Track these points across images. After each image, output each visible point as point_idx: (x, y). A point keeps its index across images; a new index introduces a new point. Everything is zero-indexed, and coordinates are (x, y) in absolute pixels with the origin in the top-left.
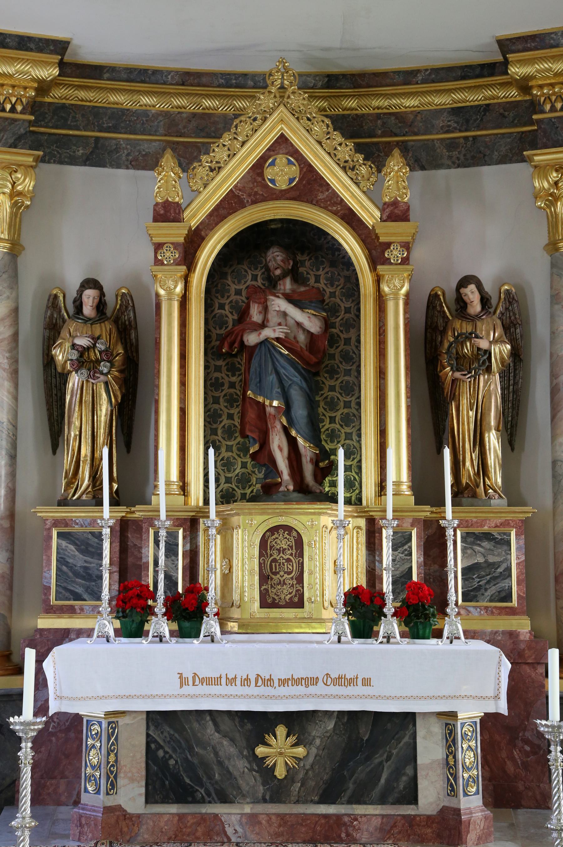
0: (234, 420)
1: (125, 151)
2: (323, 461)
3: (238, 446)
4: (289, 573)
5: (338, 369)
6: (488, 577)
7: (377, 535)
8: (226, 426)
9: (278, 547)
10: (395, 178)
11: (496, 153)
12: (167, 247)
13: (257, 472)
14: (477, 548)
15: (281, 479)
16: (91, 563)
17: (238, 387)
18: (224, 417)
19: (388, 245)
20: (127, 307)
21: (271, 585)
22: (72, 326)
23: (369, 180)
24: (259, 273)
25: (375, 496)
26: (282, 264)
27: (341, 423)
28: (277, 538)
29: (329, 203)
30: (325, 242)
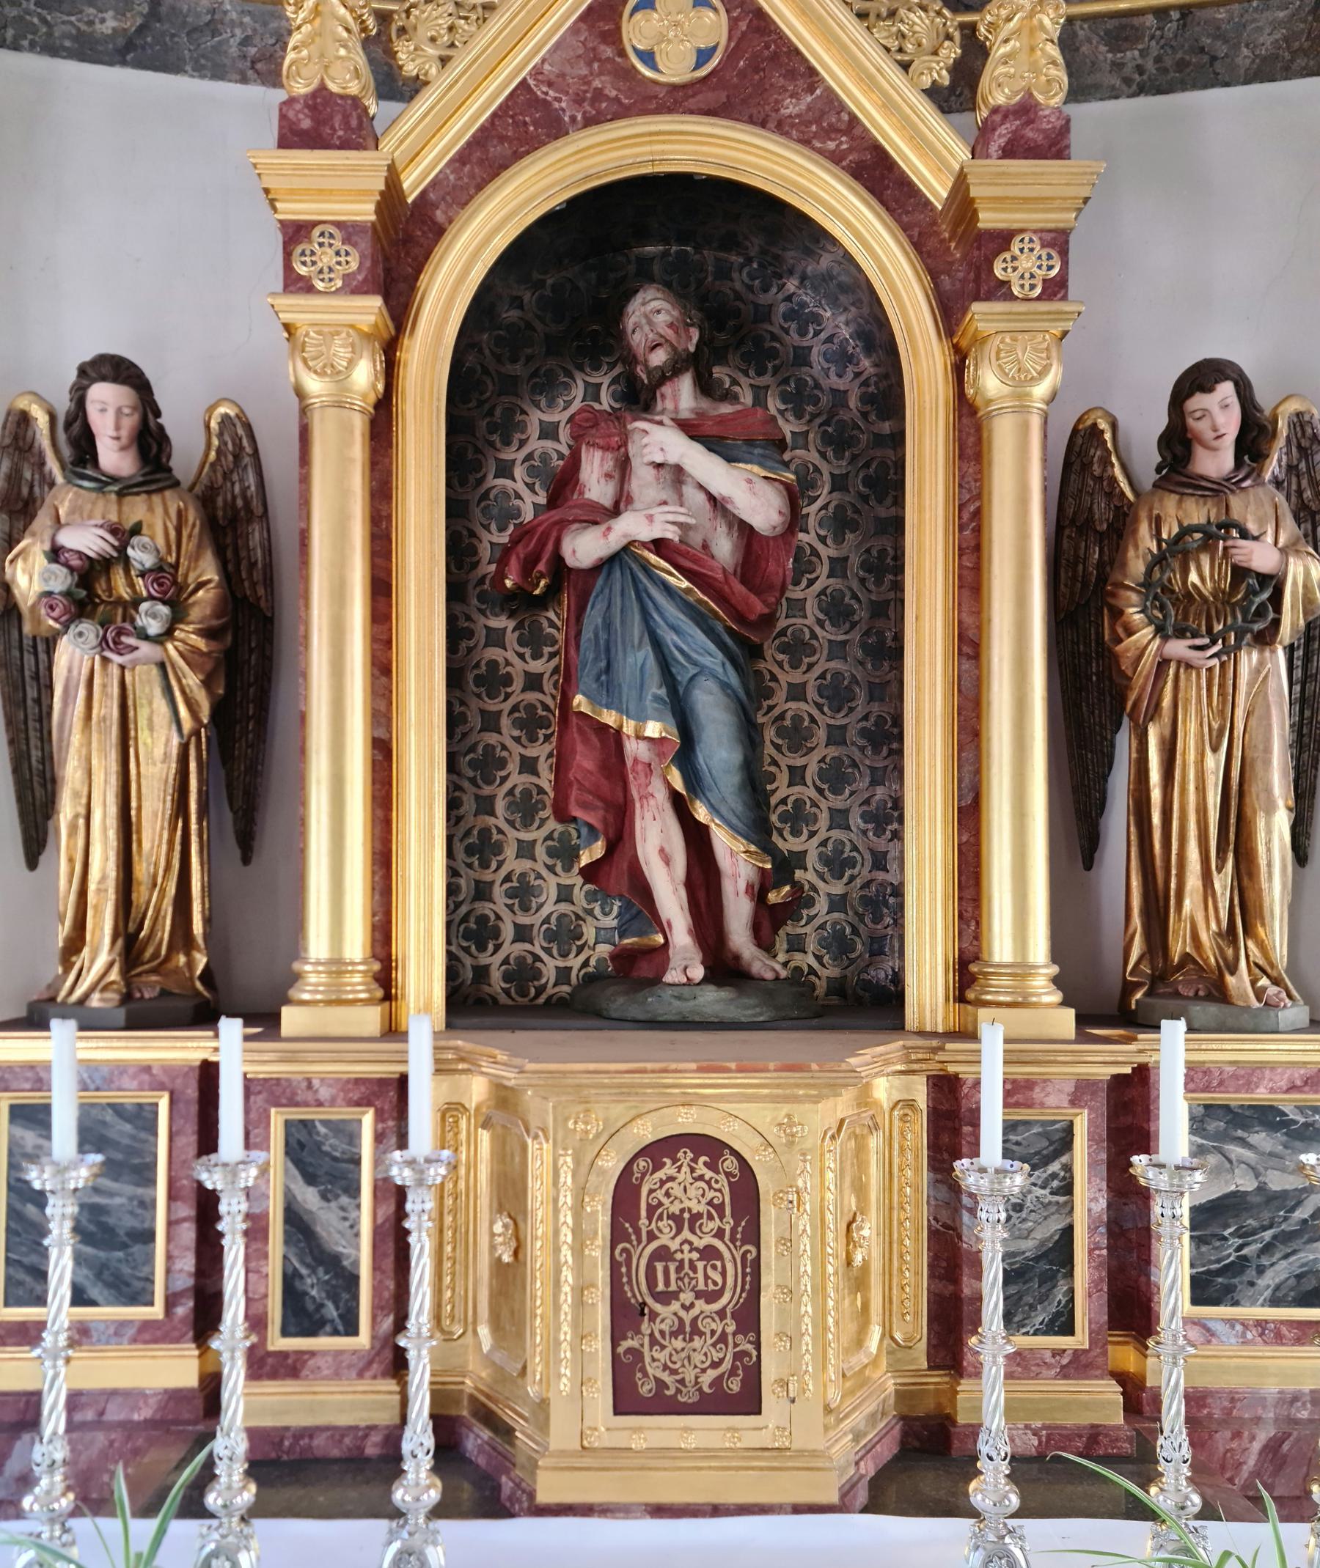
0: (538, 775)
1: (238, 31)
2: (777, 886)
3: (550, 843)
4: (711, 1297)
5: (814, 642)
6: (1267, 1235)
7: (967, 1129)
8: (517, 791)
9: (675, 1209)
10: (1025, 32)
11: (1245, 51)
12: (322, 234)
13: (597, 911)
14: (1236, 1151)
15: (666, 937)
16: (111, 1194)
17: (548, 686)
18: (513, 766)
19: (1003, 239)
20: (237, 457)
21: (652, 1335)
22: (65, 498)
23: (935, 53)
24: (604, 380)
25: (947, 999)
26: (670, 333)
27: (818, 783)
28: (671, 1179)
29: (814, 128)
30: (780, 296)
